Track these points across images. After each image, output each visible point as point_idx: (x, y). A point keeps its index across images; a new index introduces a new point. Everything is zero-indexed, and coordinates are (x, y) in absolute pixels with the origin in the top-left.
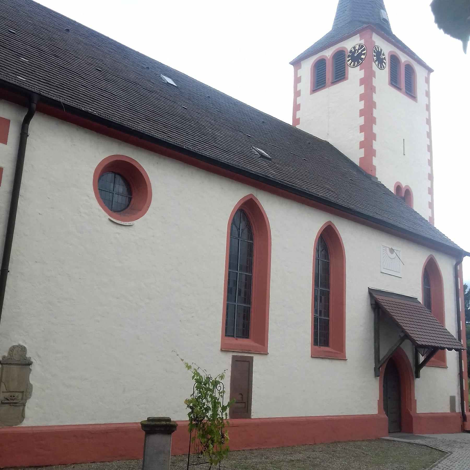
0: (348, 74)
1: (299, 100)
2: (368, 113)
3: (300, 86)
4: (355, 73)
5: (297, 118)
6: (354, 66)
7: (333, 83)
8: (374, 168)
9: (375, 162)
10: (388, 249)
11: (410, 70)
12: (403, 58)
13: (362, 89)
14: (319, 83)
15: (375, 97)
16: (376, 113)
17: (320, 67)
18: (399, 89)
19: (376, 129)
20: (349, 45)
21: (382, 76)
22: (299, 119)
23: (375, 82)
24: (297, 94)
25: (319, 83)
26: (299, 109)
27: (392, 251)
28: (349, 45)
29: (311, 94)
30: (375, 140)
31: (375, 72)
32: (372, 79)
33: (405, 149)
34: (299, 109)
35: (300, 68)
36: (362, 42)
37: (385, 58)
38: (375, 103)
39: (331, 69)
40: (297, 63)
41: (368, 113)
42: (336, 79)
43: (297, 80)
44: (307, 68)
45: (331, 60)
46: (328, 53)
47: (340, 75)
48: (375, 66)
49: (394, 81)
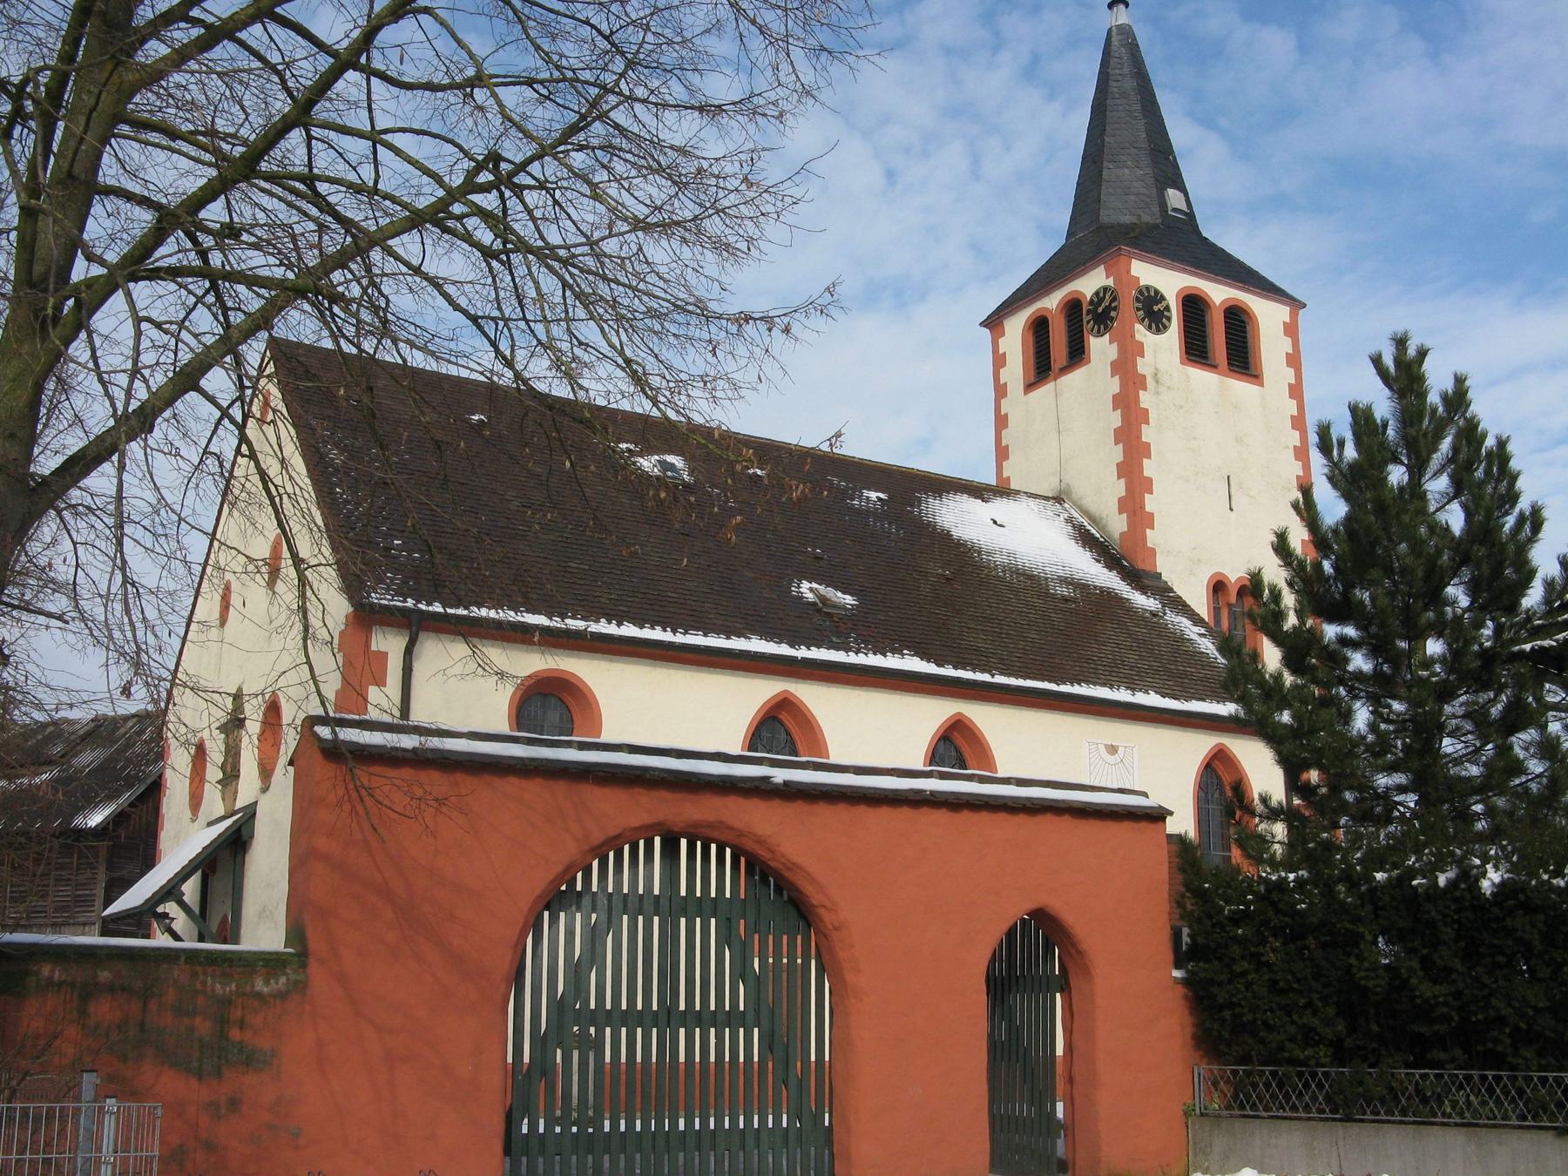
3: (1004, 375)
4: (1101, 348)
6: (1100, 334)
8: (1152, 553)
9: (1152, 538)
10: (1102, 748)
11: (1237, 319)
13: (1114, 386)
14: (1041, 369)
18: (1213, 367)
19: (1149, 468)
20: (1089, 284)
21: (1162, 349)
23: (1143, 366)
24: (1001, 391)
25: (1041, 369)
27: (1112, 750)
28: (1089, 284)
36: (1110, 282)
37: (1167, 308)
40: (994, 322)
43: (999, 361)
44: (1015, 327)
47: (1078, 354)
48: (1141, 332)
49: (1196, 350)
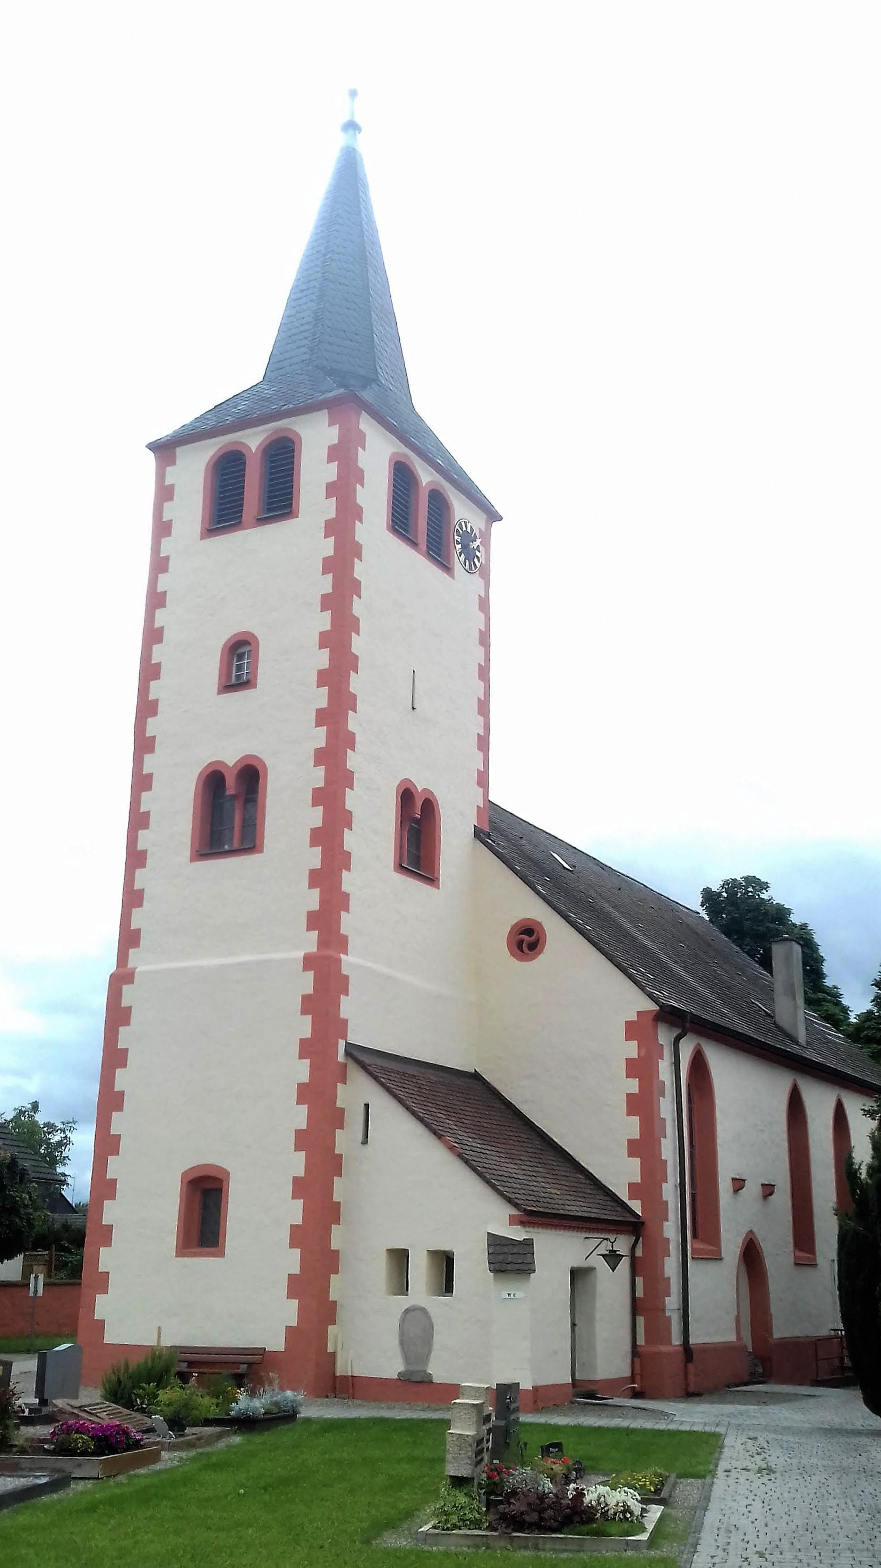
0: (299, 475)
1: (161, 618)
2: (340, 598)
5: (157, 625)
7: (262, 521)
11: (439, 503)
12: (426, 476)
14: (225, 513)
15: (360, 570)
16: (358, 607)
17: (227, 477)
18: (414, 544)
22: (158, 665)
24: (162, 528)
25: (225, 513)
26: (154, 713)
29: (202, 538)
30: (348, 869)
31: (364, 435)
32: (357, 450)
33: (416, 691)
34: (142, 864)
35: (173, 463)
38: (357, 620)
39: (257, 476)
40: (165, 450)
41: (340, 598)
42: (269, 510)
43: (165, 493)
45: (259, 455)
46: (253, 441)
